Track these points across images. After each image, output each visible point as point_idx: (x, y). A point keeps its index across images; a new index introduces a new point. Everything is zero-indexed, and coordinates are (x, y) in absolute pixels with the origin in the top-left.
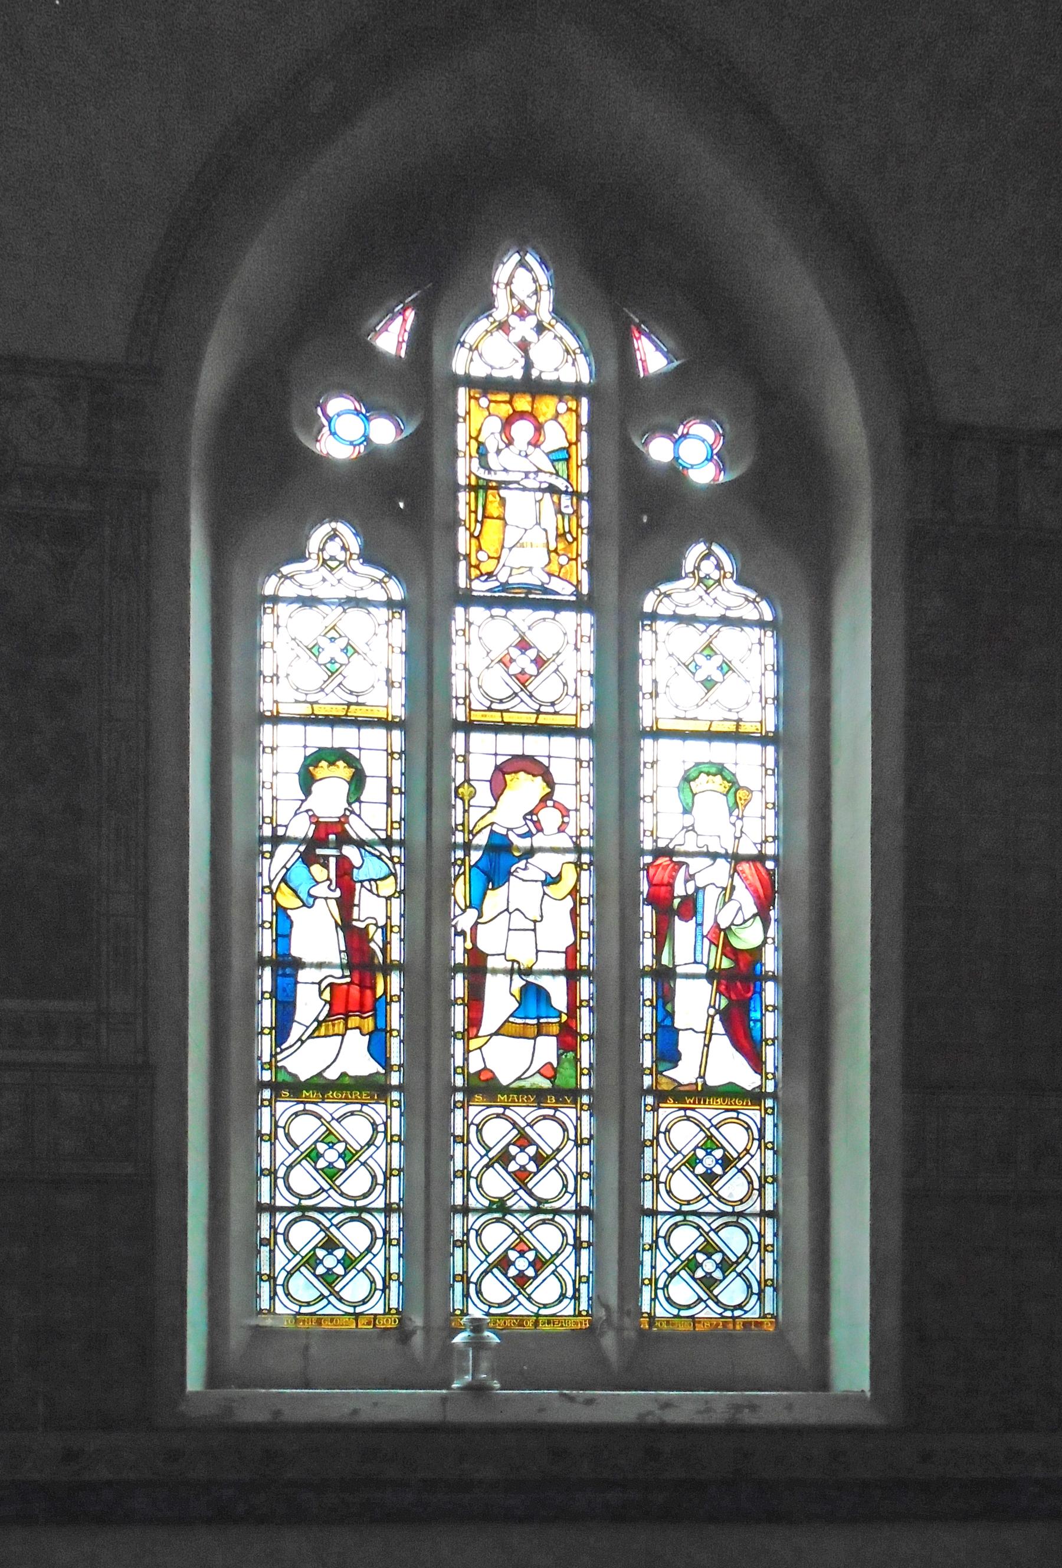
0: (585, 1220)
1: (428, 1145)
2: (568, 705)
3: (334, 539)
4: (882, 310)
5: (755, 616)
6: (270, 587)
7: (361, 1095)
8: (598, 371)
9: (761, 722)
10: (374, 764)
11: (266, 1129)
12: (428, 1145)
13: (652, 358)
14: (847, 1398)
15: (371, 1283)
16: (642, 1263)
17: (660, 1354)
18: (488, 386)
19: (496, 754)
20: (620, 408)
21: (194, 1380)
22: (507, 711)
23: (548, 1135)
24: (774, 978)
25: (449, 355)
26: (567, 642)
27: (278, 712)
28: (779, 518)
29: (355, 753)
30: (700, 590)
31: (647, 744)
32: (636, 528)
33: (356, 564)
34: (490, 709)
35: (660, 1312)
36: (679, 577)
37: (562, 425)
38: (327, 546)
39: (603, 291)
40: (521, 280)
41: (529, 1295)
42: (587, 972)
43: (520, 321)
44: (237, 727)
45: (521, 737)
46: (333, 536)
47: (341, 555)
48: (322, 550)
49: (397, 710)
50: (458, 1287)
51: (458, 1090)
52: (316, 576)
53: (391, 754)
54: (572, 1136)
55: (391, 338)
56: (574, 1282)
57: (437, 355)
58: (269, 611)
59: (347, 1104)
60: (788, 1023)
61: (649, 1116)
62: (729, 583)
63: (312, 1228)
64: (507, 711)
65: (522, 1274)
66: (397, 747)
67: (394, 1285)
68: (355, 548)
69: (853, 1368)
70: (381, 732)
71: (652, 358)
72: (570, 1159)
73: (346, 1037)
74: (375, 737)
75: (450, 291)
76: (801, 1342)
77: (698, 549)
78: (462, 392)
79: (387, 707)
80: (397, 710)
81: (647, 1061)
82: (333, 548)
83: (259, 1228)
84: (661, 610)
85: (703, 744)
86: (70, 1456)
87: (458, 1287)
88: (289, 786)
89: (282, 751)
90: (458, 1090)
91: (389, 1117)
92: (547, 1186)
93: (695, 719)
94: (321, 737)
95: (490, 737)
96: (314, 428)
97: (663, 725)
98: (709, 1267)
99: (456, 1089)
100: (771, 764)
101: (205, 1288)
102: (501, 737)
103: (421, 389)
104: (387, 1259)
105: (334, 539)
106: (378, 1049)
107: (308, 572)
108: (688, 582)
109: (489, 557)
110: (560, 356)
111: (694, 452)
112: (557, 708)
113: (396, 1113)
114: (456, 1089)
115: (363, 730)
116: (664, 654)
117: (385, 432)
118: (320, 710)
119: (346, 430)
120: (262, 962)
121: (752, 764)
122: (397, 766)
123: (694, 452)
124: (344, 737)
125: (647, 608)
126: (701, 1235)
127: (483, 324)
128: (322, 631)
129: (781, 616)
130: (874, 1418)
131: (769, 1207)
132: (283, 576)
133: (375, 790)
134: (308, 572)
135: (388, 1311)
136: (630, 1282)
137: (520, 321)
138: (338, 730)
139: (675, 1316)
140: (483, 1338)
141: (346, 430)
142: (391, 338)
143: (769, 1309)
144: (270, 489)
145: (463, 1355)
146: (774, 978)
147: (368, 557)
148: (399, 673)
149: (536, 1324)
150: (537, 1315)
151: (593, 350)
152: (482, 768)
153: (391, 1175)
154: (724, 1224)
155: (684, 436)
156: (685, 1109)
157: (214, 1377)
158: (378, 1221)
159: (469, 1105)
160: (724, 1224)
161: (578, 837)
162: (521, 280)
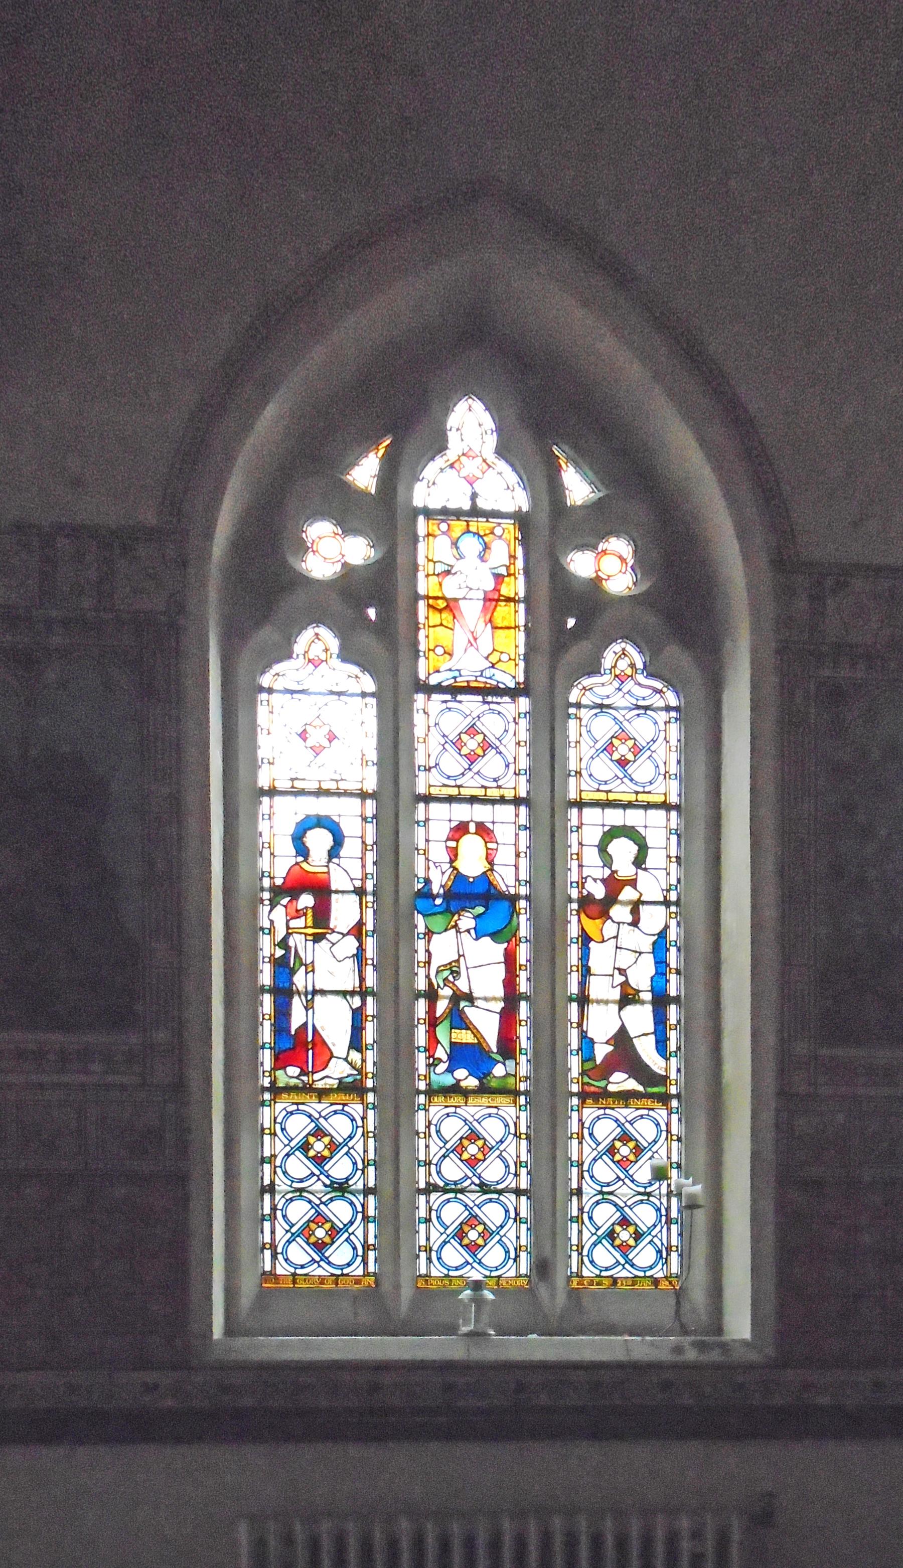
0: (523, 1199)
2: (509, 781)
3: (317, 640)
5: (661, 704)
6: (266, 680)
7: (614, 1102)
8: (534, 500)
9: (665, 794)
10: (351, 827)
11: (421, 1128)
13: (578, 488)
15: (506, 1252)
17: (582, 1308)
18: (446, 513)
19: (603, 825)
20: (547, 530)
21: (217, 1331)
22: (610, 791)
23: (340, 1126)
25: (410, 489)
26: (507, 724)
27: (581, 799)
28: (677, 619)
29: (490, 826)
30: (616, 684)
32: (566, 630)
33: (640, 678)
34: (598, 790)
35: (434, 1273)
36: (289, 656)
37: (504, 548)
38: (618, 663)
40: (470, 423)
41: (480, 1260)
43: (471, 458)
45: (469, 806)
46: (624, 653)
47: (629, 672)
48: (615, 666)
49: (371, 785)
50: (423, 1255)
52: (609, 690)
53: (364, 819)
54: (512, 1131)
55: (365, 473)
56: (516, 1249)
57: (401, 490)
58: (265, 703)
59: (637, 1109)
61: (421, 1114)
62: (335, 662)
63: (298, 1208)
64: (610, 791)
65: (474, 1247)
66: (674, 825)
67: (523, 1255)
68: (640, 665)
69: (739, 1325)
70: (662, 813)
71: (578, 488)
72: (511, 1148)
74: (658, 816)
75: (413, 433)
76: (698, 1296)
77: (308, 634)
78: (421, 519)
79: (515, 788)
80: (371, 785)
81: (267, 1066)
82: (623, 664)
84: (584, 701)
85: (312, 799)
86: (877, 1385)
87: (423, 1255)
91: (518, 1118)
92: (492, 1171)
93: (649, 792)
94: (615, 817)
95: (598, 811)
96: (302, 548)
97: (434, 791)
98: (320, 1235)
99: (419, 1092)
102: (608, 811)
103: (387, 516)
104: (273, 1232)
105: (317, 640)
107: (603, 685)
108: (606, 678)
109: (500, 660)
110: (505, 490)
111: (611, 566)
112: (500, 783)
113: (675, 1117)
114: (419, 1092)
115: (628, 811)
116: (586, 739)
117: (359, 551)
118: (465, 792)
119: (330, 550)
120: (263, 990)
122: (370, 829)
123: (611, 566)
124: (634, 818)
125: (573, 699)
126: (313, 1207)
127: (439, 462)
128: (306, 725)
129: (683, 704)
130: (753, 1357)
131: (371, 1184)
132: (584, 688)
133: (351, 848)
134: (603, 685)
135: (366, 1274)
137: (471, 458)
138: (477, 807)
139: (597, 1276)
140: (482, 1295)
141: (330, 550)
142: (365, 473)
143: (371, 1268)
144: (268, 599)
145: (467, 1307)
146: (527, 998)
147: (346, 655)
148: (373, 756)
149: (294, 1282)
150: (294, 1275)
151: (528, 483)
152: (440, 830)
153: (368, 1164)
154: (638, 1214)
155: (604, 552)
156: (297, 1104)
157: (229, 1331)
158: (358, 1201)
159: (583, 1107)
160: (638, 1214)
161: (668, 891)
162: (470, 423)
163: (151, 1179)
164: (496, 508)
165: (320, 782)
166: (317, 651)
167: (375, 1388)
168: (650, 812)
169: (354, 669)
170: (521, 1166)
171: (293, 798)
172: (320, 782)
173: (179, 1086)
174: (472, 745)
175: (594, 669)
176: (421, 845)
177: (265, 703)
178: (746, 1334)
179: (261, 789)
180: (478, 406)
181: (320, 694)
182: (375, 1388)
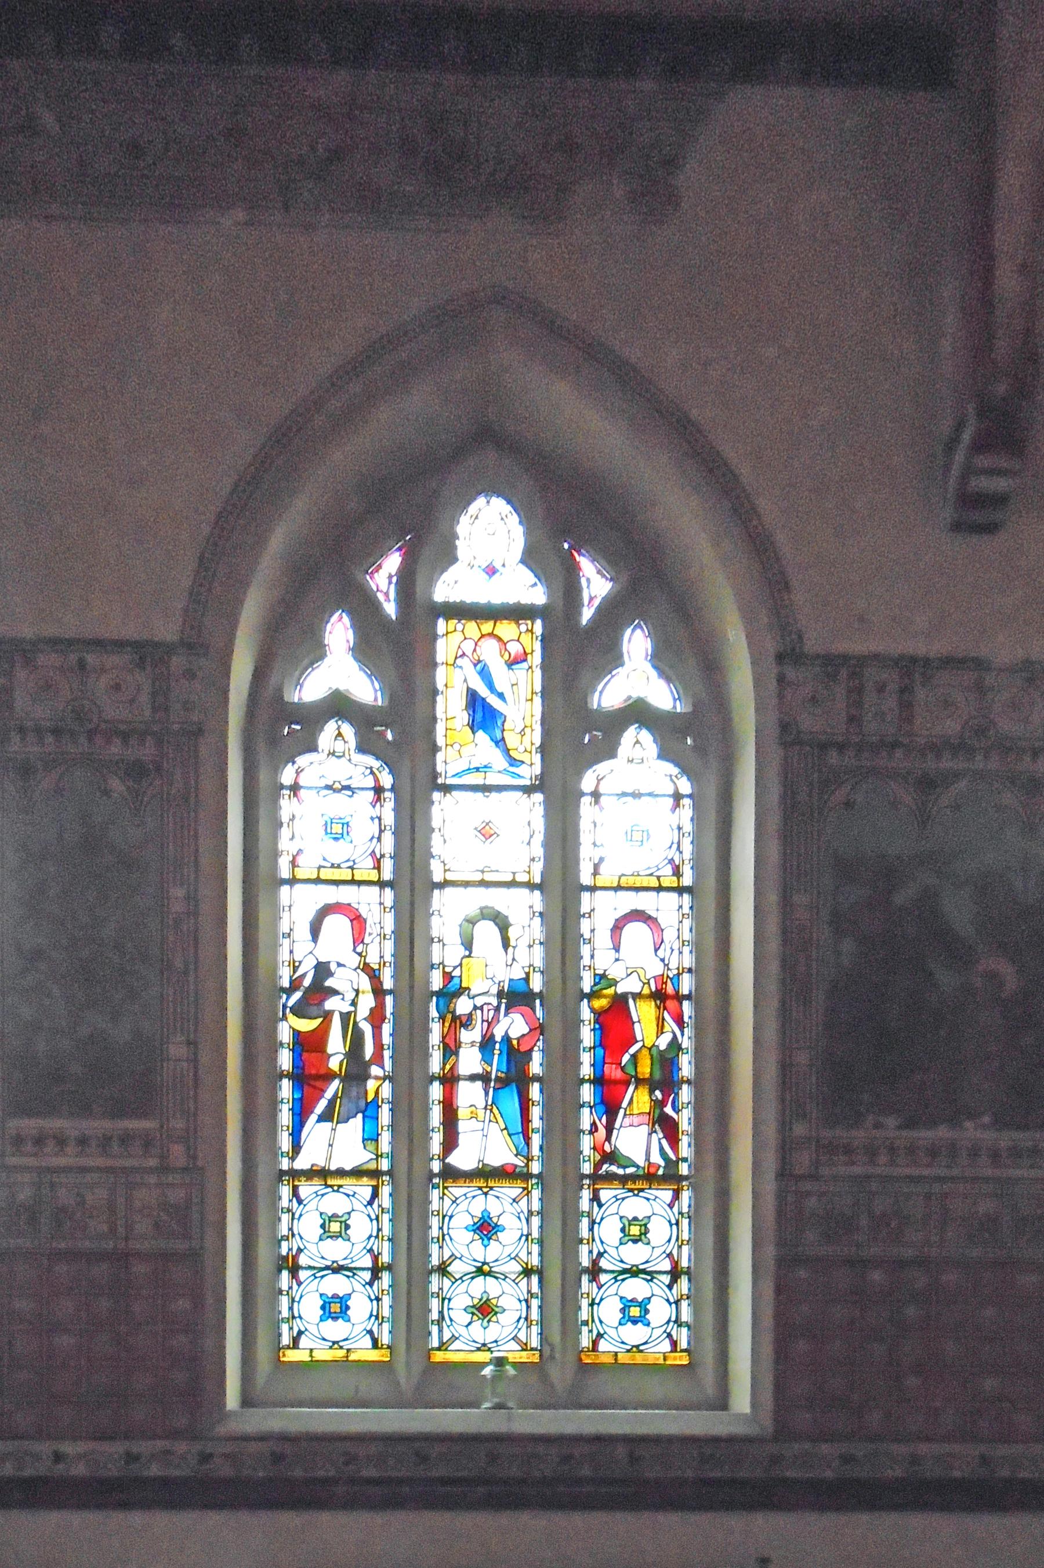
1: (412, 1223)
4: (772, 584)
8: (550, 594)
12: (412, 1223)
14: (739, 1416)
16: (580, 1308)
24: (688, 1082)
31: (585, 896)
39: (568, 514)
42: (537, 1079)
43: (489, 545)
44: (261, 881)
51: (436, 1175)
55: (384, 576)
57: (419, 589)
60: (698, 1119)
69: (741, 1401)
73: (373, 691)
75: (429, 545)
83: (280, 1335)
88: (303, 932)
89: (298, 905)
90: (436, 1175)
100: (686, 909)
101: (240, 1366)
106: (371, 1139)
120: (282, 1075)
121: (669, 909)
124: (645, 902)
128: (326, 810)
136: (570, 1325)
137: (489, 545)
146: (688, 1082)
157: (247, 1401)
163: (159, 1279)
164: (475, 601)
165: (514, 873)
166: (637, 753)
167: (278, 1458)
168: (662, 894)
169: (673, 769)
170: (438, 1238)
171: (335, 887)
172: (514, 873)
173: (193, 1169)
174: (488, 834)
175: (312, 747)
176: (587, 936)
177: (286, 797)
178: (747, 1410)
179: (434, 883)
180: (499, 504)
181: (363, 789)
182: (351, 1459)
